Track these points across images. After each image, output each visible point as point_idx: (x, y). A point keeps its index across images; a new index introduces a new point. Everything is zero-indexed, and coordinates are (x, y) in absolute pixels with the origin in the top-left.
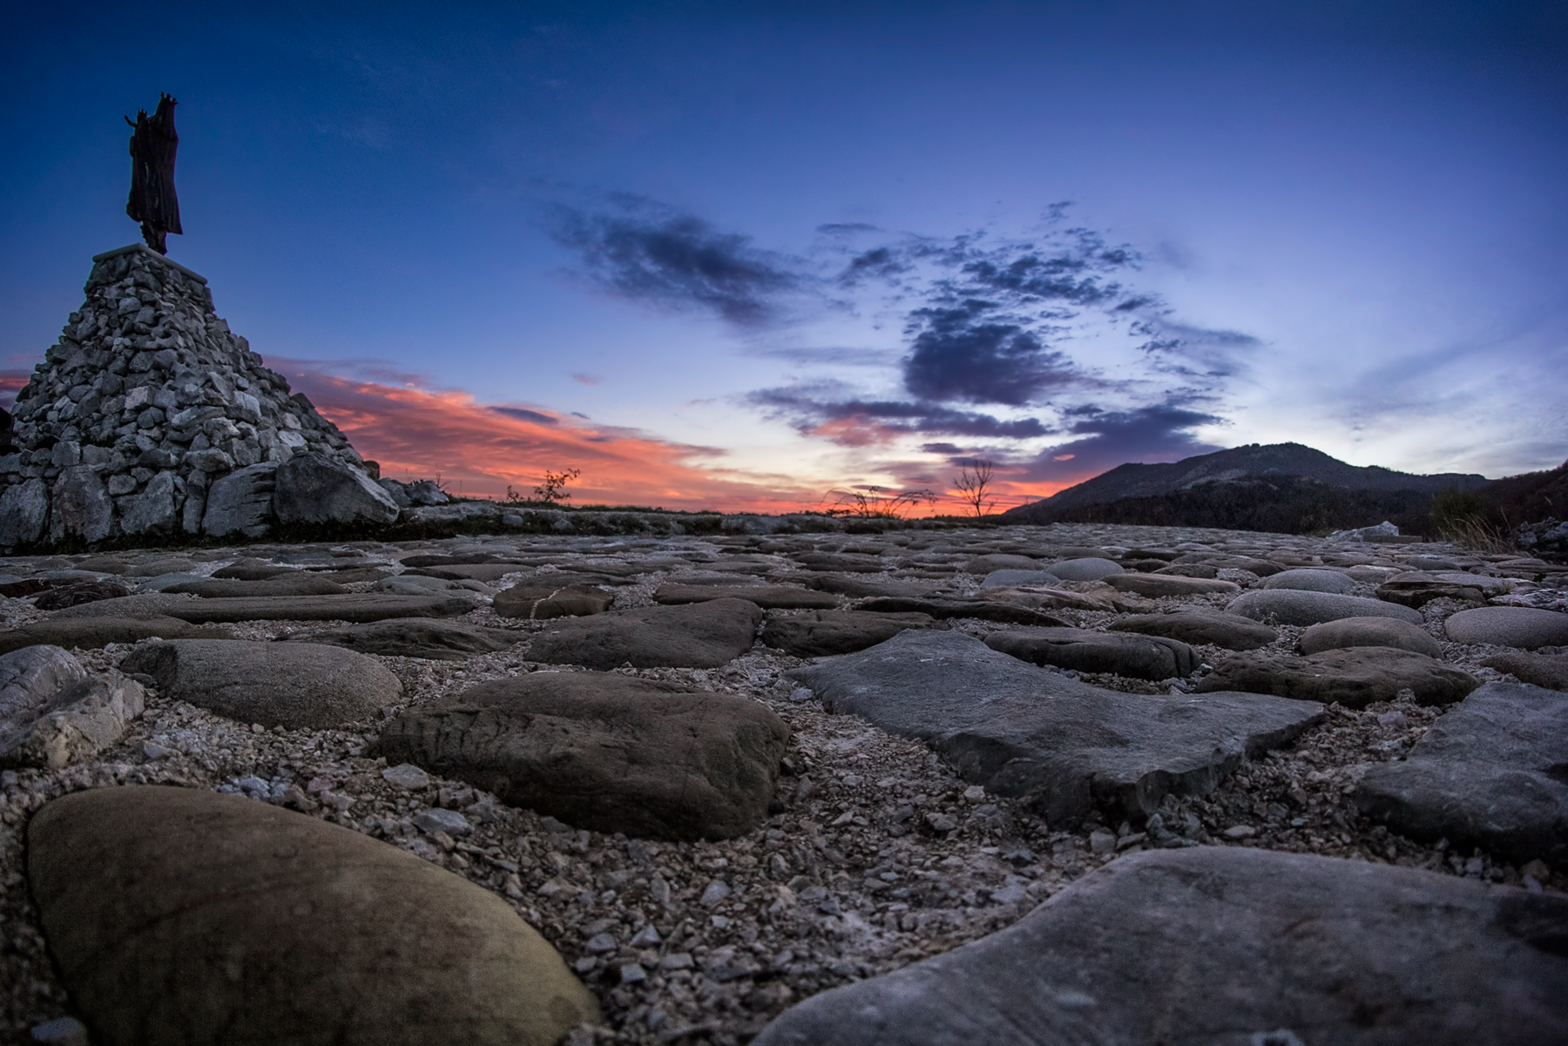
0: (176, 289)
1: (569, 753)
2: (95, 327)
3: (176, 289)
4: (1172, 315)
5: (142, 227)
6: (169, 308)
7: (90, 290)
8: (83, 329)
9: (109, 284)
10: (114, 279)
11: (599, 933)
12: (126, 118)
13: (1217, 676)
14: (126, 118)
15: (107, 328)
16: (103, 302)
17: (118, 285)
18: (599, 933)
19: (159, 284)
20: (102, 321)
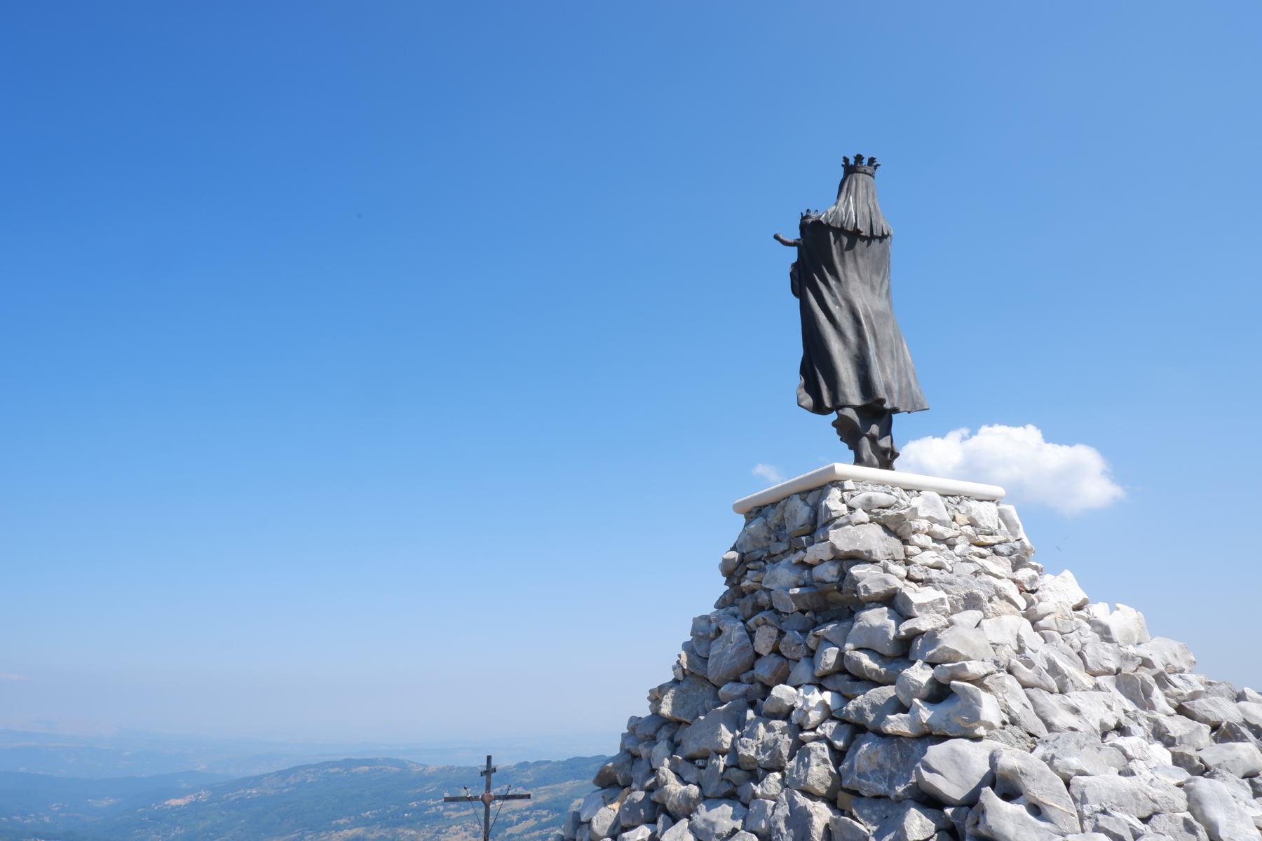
0: (937, 539)
1: (900, 514)
2: (750, 653)
3: (937, 539)
4: (1095, 728)
5: (835, 424)
6: (933, 606)
7: (733, 572)
8: (726, 653)
9: (772, 558)
10: (783, 546)
11: (1205, 721)
12: (776, 237)
13: (751, 583)
14: (776, 237)
15: (777, 661)
16: (763, 598)
17: (795, 558)
18: (1205, 721)
19: (896, 543)
20: (763, 642)
